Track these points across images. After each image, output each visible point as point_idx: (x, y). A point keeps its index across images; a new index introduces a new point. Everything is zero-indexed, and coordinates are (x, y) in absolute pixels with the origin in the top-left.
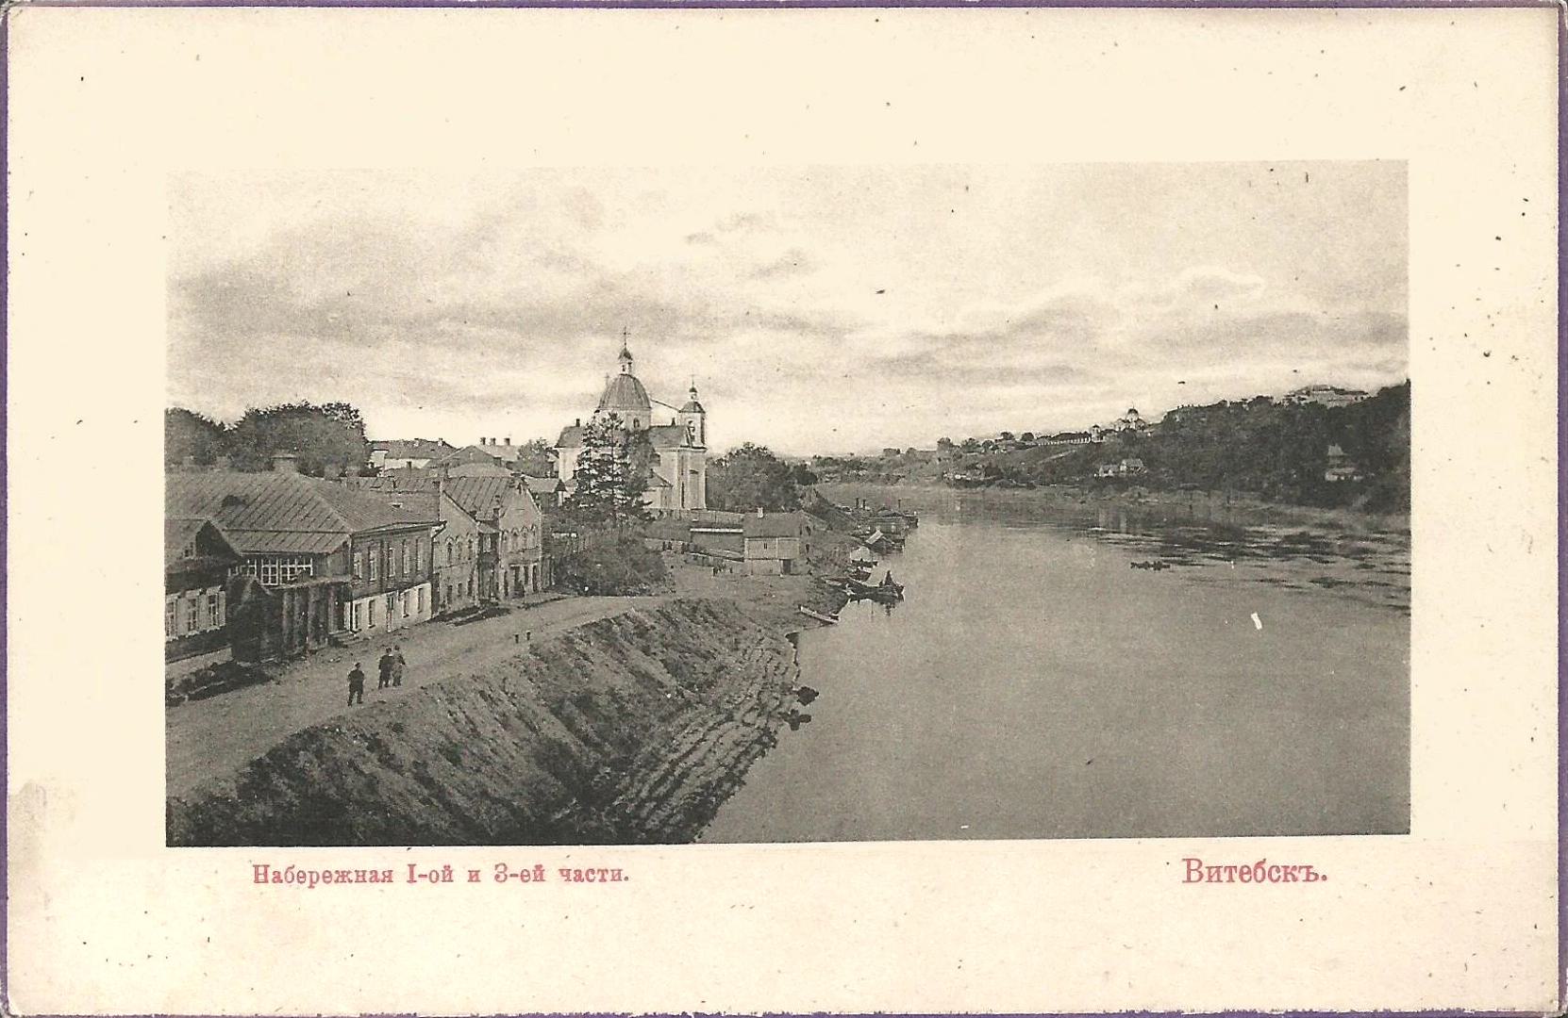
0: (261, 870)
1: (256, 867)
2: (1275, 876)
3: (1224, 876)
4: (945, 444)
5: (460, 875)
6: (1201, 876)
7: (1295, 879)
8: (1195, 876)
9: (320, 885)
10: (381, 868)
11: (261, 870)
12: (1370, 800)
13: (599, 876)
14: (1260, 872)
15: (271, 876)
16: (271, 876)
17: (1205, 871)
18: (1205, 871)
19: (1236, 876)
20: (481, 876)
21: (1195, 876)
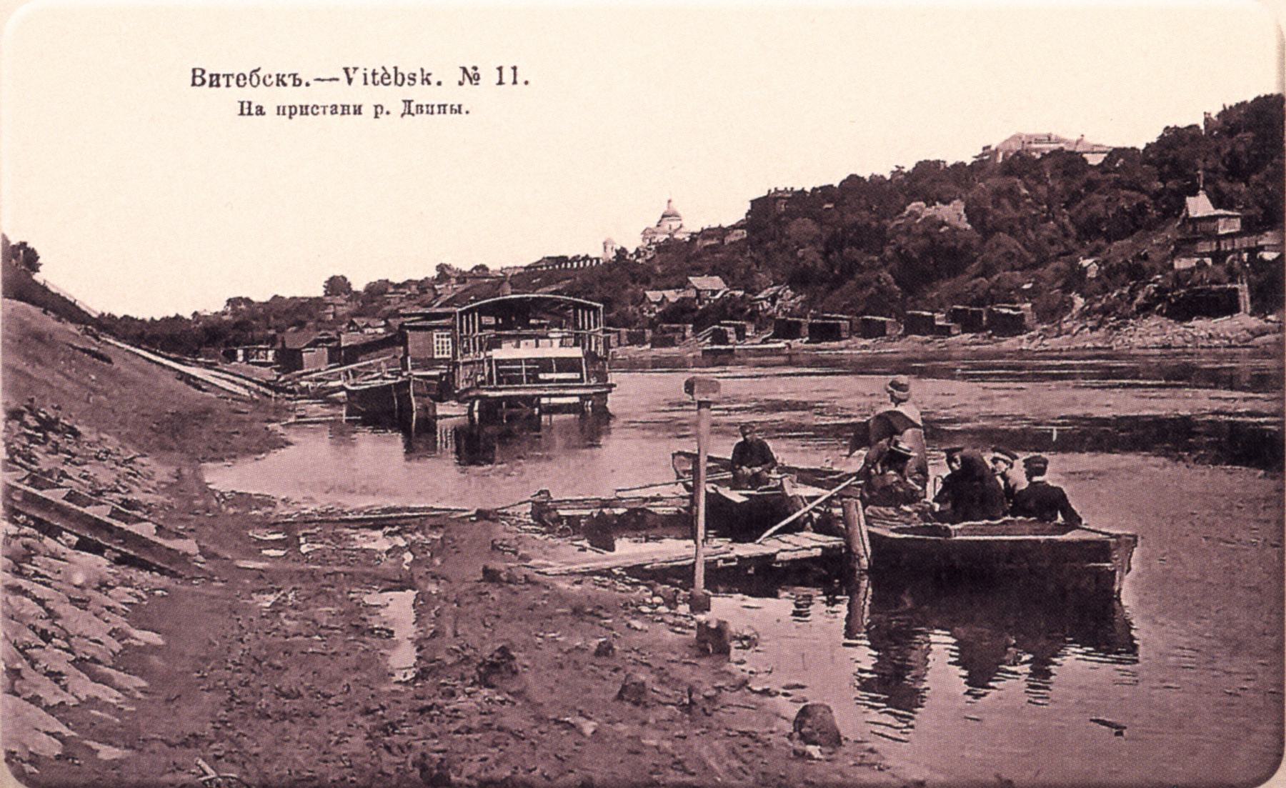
0: (246, 105)
1: (242, 103)
2: (268, 81)
3: (223, 81)
4: (337, 285)
5: (368, 110)
6: (204, 82)
7: (285, 85)
8: (198, 81)
9: (297, 117)
10: (351, 102)
11: (246, 105)
12: (707, 563)
13: (321, 110)
14: (255, 78)
15: (253, 110)
16: (253, 110)
17: (206, 77)
18: (206, 77)
19: (233, 81)
20: (363, 110)
21: (198, 81)
